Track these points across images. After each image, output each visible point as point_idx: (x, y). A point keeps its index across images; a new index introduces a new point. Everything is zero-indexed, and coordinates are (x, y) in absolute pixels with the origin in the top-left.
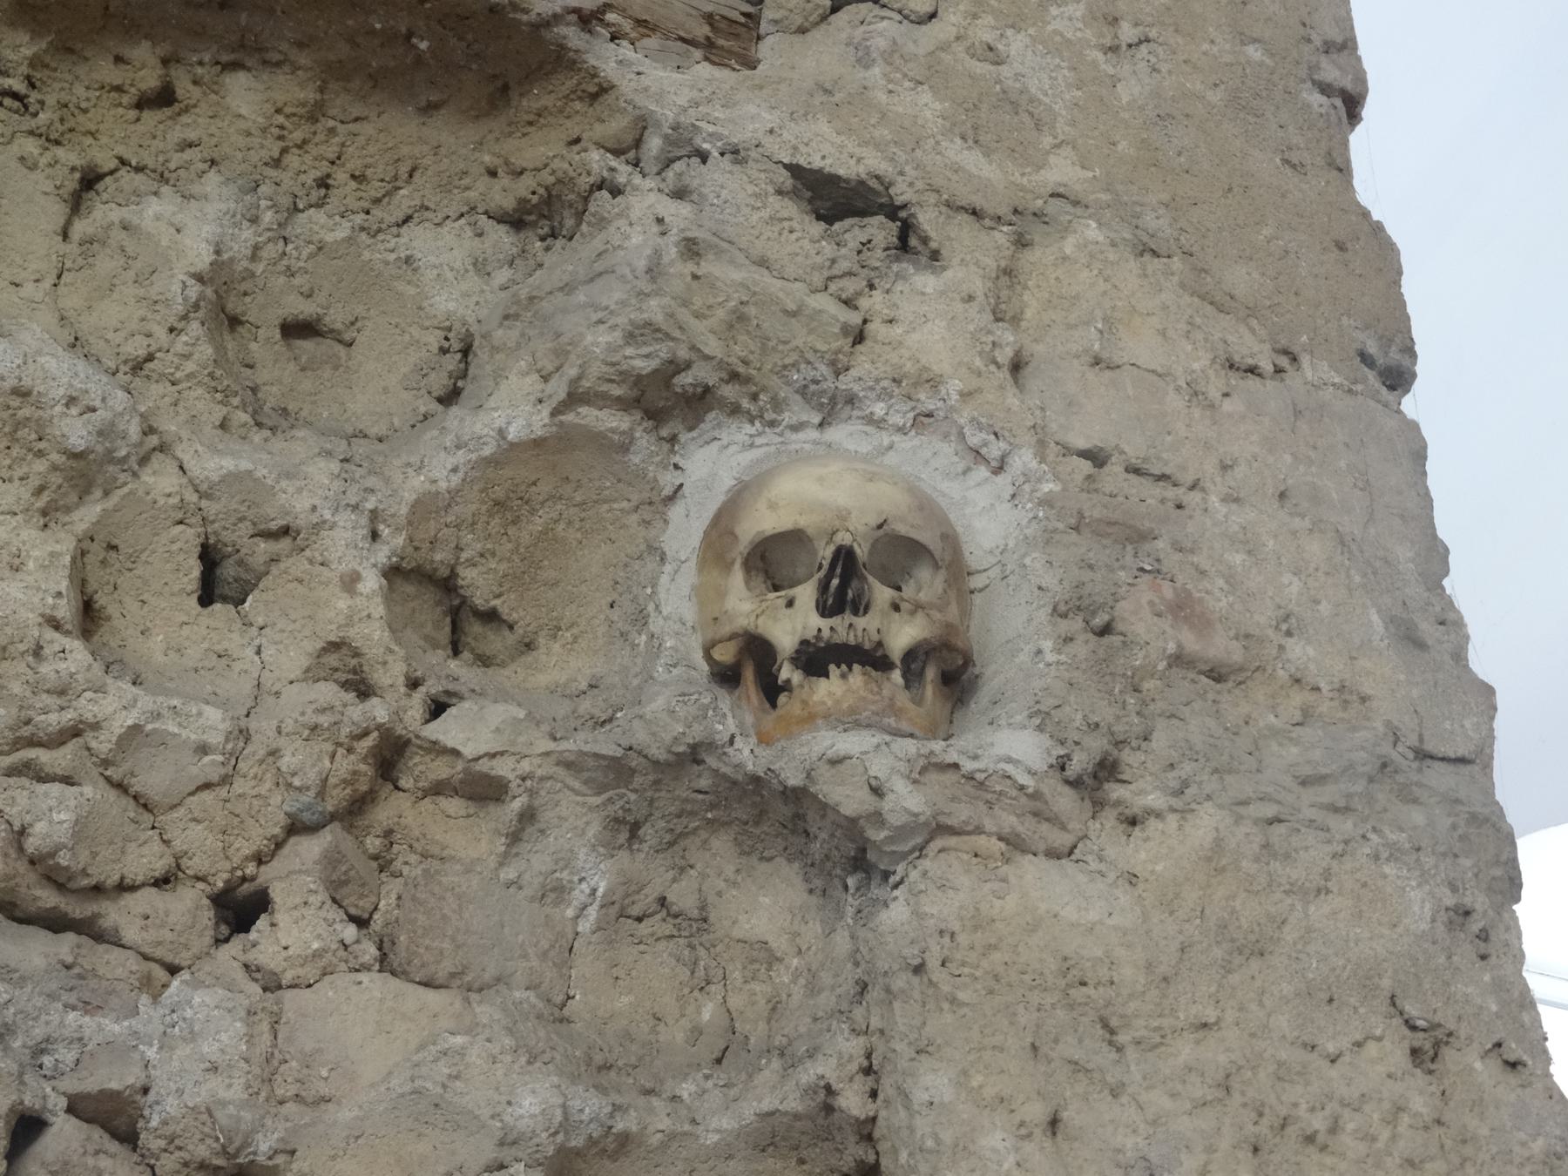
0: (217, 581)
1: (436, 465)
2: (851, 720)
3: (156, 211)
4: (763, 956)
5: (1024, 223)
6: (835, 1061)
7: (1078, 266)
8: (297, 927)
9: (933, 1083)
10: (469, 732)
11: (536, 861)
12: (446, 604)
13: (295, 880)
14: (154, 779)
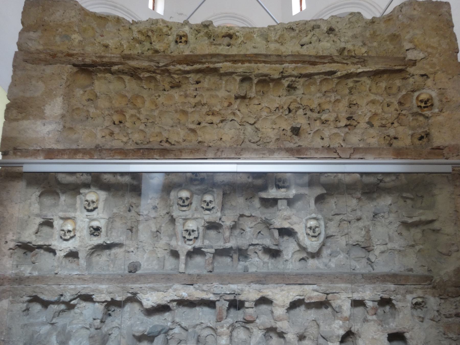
0: (388, 106)
1: (399, 96)
2: (427, 111)
3: (381, 84)
4: (421, 121)
5: (435, 73)
6: (427, 129)
7: (440, 75)
8: (396, 124)
9: (433, 131)
10: (404, 112)
11: (408, 118)
12: (400, 103)
13: (395, 122)
14: (388, 119)
